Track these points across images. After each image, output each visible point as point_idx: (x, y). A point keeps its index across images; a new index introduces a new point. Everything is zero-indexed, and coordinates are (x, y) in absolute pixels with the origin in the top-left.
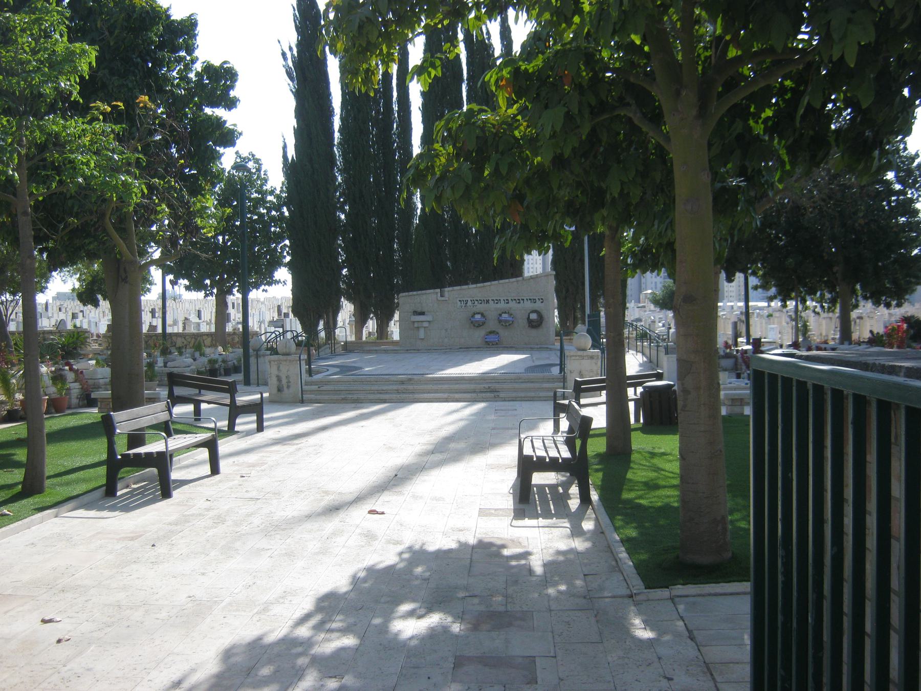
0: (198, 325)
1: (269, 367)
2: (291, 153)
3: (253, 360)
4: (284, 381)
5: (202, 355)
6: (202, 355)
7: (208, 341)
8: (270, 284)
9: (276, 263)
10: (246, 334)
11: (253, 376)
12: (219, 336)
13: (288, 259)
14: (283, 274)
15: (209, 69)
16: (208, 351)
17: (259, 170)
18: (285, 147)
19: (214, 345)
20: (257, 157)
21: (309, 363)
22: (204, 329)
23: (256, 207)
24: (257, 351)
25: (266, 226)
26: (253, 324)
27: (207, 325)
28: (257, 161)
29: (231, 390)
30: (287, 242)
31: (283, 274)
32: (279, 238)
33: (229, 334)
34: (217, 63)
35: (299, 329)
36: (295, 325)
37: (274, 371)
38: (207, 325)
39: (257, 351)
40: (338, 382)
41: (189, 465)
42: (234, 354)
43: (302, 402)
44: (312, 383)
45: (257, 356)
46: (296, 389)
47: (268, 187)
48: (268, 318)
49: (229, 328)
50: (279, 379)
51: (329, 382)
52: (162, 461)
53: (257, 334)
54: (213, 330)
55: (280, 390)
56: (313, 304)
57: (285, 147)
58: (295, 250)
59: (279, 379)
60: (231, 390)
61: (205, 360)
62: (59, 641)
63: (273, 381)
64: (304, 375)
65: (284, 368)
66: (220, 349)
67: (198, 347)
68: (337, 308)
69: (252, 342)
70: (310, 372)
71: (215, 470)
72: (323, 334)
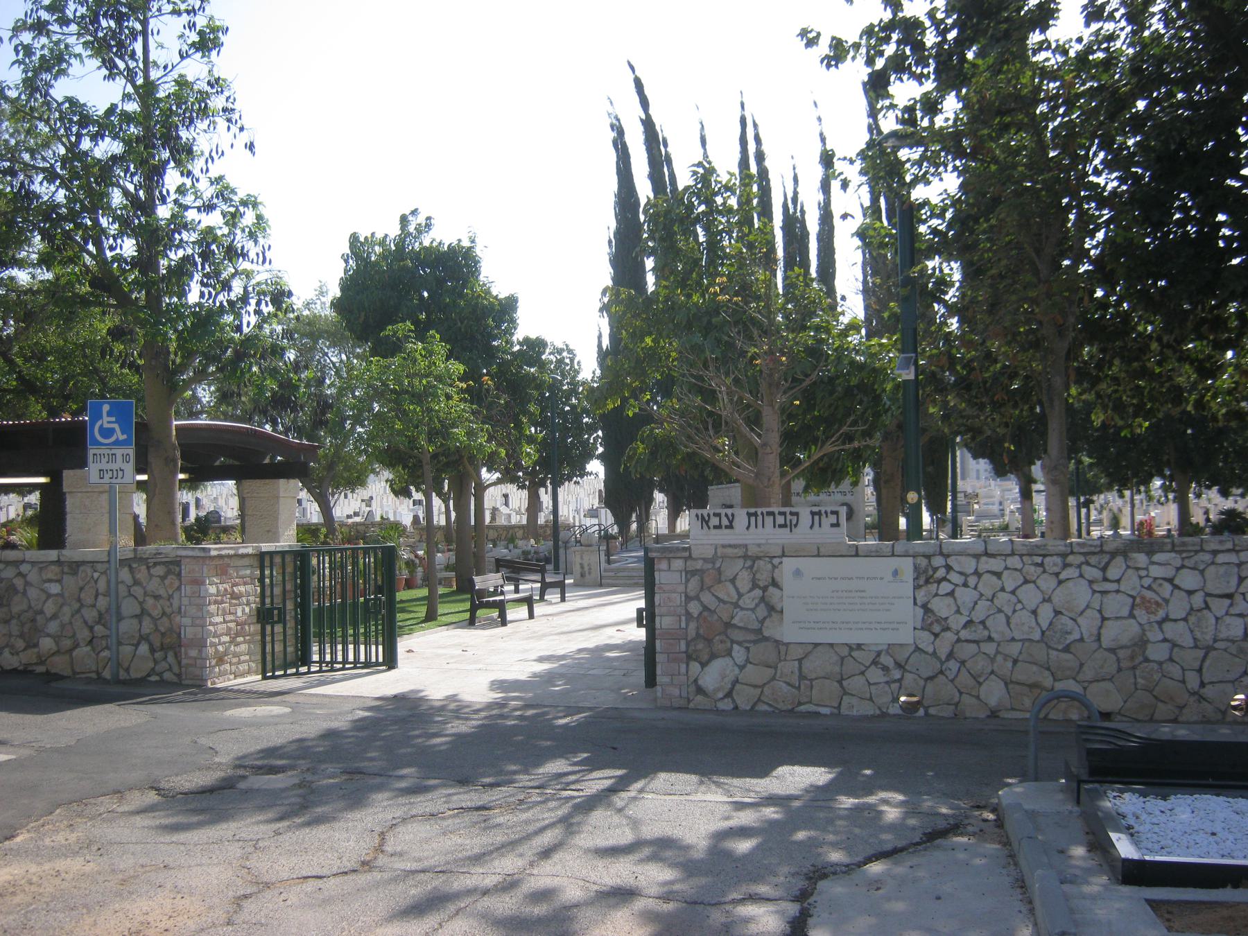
0: (509, 516)
1: (575, 557)
2: (606, 342)
3: (562, 551)
4: (586, 569)
5: (515, 547)
6: (515, 547)
7: (520, 533)
8: (582, 476)
9: (588, 455)
10: (556, 525)
11: (562, 565)
12: (532, 529)
13: (601, 450)
14: (596, 467)
15: (526, 341)
16: (520, 543)
17: (572, 360)
18: (600, 337)
19: (526, 538)
20: (571, 347)
21: (608, 554)
22: (515, 520)
23: (568, 399)
24: (566, 543)
25: (578, 419)
26: (563, 511)
27: (520, 519)
28: (570, 351)
29: (542, 571)
30: (600, 433)
31: (596, 467)
32: (591, 429)
33: (541, 526)
34: (533, 336)
35: (611, 519)
36: (607, 518)
37: (577, 560)
38: (520, 519)
39: (566, 543)
40: (633, 569)
41: (517, 613)
42: (545, 546)
43: (601, 585)
44: (611, 571)
45: (566, 548)
46: (595, 575)
47: (580, 378)
48: (587, 506)
49: (541, 520)
50: (582, 567)
51: (624, 570)
52: (501, 607)
53: (569, 527)
54: (524, 522)
55: (582, 575)
56: (624, 496)
57: (600, 337)
58: (606, 442)
59: (582, 567)
60: (542, 571)
61: (518, 551)
62: (819, 119)
63: (577, 569)
64: (604, 565)
65: (586, 558)
66: (532, 541)
67: (512, 540)
68: (651, 500)
69: (563, 535)
70: (609, 562)
71: (531, 616)
72: (634, 526)
